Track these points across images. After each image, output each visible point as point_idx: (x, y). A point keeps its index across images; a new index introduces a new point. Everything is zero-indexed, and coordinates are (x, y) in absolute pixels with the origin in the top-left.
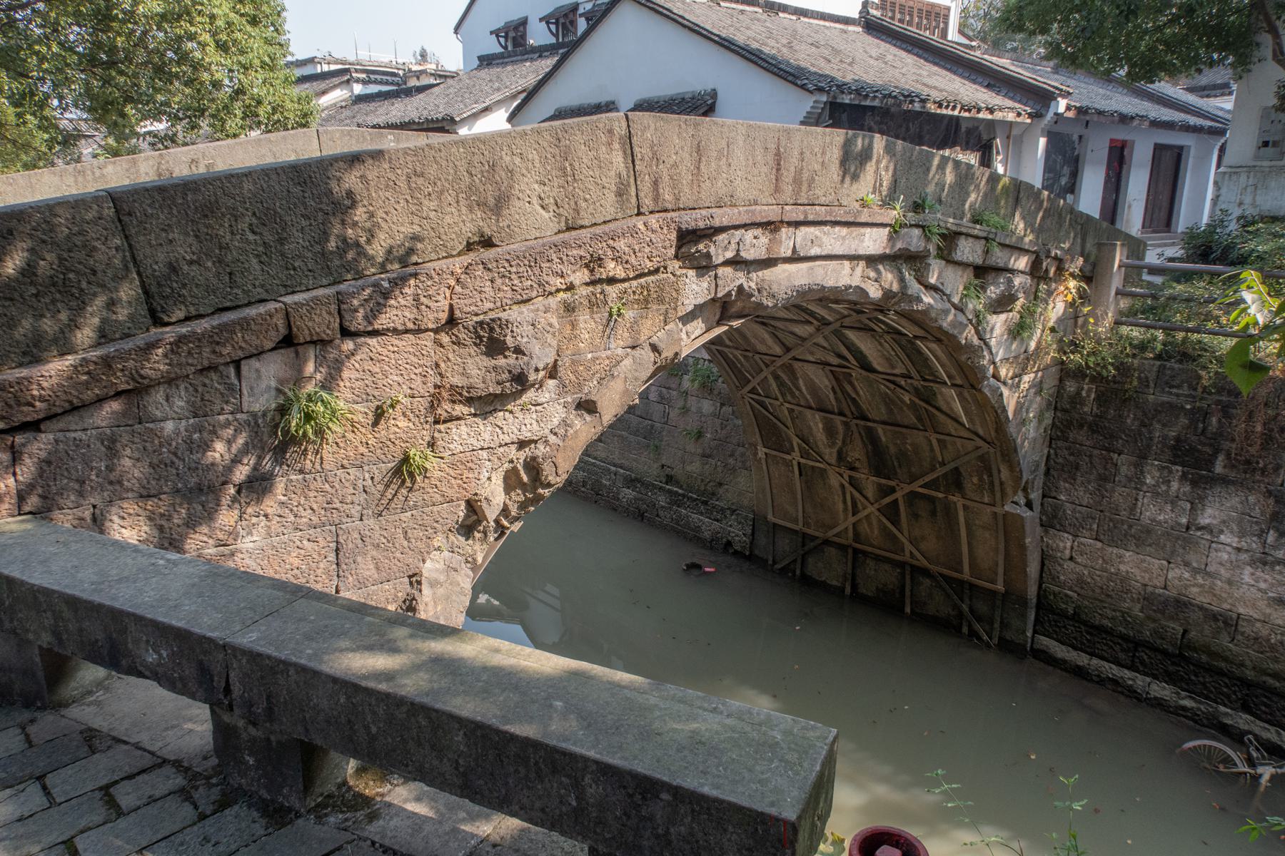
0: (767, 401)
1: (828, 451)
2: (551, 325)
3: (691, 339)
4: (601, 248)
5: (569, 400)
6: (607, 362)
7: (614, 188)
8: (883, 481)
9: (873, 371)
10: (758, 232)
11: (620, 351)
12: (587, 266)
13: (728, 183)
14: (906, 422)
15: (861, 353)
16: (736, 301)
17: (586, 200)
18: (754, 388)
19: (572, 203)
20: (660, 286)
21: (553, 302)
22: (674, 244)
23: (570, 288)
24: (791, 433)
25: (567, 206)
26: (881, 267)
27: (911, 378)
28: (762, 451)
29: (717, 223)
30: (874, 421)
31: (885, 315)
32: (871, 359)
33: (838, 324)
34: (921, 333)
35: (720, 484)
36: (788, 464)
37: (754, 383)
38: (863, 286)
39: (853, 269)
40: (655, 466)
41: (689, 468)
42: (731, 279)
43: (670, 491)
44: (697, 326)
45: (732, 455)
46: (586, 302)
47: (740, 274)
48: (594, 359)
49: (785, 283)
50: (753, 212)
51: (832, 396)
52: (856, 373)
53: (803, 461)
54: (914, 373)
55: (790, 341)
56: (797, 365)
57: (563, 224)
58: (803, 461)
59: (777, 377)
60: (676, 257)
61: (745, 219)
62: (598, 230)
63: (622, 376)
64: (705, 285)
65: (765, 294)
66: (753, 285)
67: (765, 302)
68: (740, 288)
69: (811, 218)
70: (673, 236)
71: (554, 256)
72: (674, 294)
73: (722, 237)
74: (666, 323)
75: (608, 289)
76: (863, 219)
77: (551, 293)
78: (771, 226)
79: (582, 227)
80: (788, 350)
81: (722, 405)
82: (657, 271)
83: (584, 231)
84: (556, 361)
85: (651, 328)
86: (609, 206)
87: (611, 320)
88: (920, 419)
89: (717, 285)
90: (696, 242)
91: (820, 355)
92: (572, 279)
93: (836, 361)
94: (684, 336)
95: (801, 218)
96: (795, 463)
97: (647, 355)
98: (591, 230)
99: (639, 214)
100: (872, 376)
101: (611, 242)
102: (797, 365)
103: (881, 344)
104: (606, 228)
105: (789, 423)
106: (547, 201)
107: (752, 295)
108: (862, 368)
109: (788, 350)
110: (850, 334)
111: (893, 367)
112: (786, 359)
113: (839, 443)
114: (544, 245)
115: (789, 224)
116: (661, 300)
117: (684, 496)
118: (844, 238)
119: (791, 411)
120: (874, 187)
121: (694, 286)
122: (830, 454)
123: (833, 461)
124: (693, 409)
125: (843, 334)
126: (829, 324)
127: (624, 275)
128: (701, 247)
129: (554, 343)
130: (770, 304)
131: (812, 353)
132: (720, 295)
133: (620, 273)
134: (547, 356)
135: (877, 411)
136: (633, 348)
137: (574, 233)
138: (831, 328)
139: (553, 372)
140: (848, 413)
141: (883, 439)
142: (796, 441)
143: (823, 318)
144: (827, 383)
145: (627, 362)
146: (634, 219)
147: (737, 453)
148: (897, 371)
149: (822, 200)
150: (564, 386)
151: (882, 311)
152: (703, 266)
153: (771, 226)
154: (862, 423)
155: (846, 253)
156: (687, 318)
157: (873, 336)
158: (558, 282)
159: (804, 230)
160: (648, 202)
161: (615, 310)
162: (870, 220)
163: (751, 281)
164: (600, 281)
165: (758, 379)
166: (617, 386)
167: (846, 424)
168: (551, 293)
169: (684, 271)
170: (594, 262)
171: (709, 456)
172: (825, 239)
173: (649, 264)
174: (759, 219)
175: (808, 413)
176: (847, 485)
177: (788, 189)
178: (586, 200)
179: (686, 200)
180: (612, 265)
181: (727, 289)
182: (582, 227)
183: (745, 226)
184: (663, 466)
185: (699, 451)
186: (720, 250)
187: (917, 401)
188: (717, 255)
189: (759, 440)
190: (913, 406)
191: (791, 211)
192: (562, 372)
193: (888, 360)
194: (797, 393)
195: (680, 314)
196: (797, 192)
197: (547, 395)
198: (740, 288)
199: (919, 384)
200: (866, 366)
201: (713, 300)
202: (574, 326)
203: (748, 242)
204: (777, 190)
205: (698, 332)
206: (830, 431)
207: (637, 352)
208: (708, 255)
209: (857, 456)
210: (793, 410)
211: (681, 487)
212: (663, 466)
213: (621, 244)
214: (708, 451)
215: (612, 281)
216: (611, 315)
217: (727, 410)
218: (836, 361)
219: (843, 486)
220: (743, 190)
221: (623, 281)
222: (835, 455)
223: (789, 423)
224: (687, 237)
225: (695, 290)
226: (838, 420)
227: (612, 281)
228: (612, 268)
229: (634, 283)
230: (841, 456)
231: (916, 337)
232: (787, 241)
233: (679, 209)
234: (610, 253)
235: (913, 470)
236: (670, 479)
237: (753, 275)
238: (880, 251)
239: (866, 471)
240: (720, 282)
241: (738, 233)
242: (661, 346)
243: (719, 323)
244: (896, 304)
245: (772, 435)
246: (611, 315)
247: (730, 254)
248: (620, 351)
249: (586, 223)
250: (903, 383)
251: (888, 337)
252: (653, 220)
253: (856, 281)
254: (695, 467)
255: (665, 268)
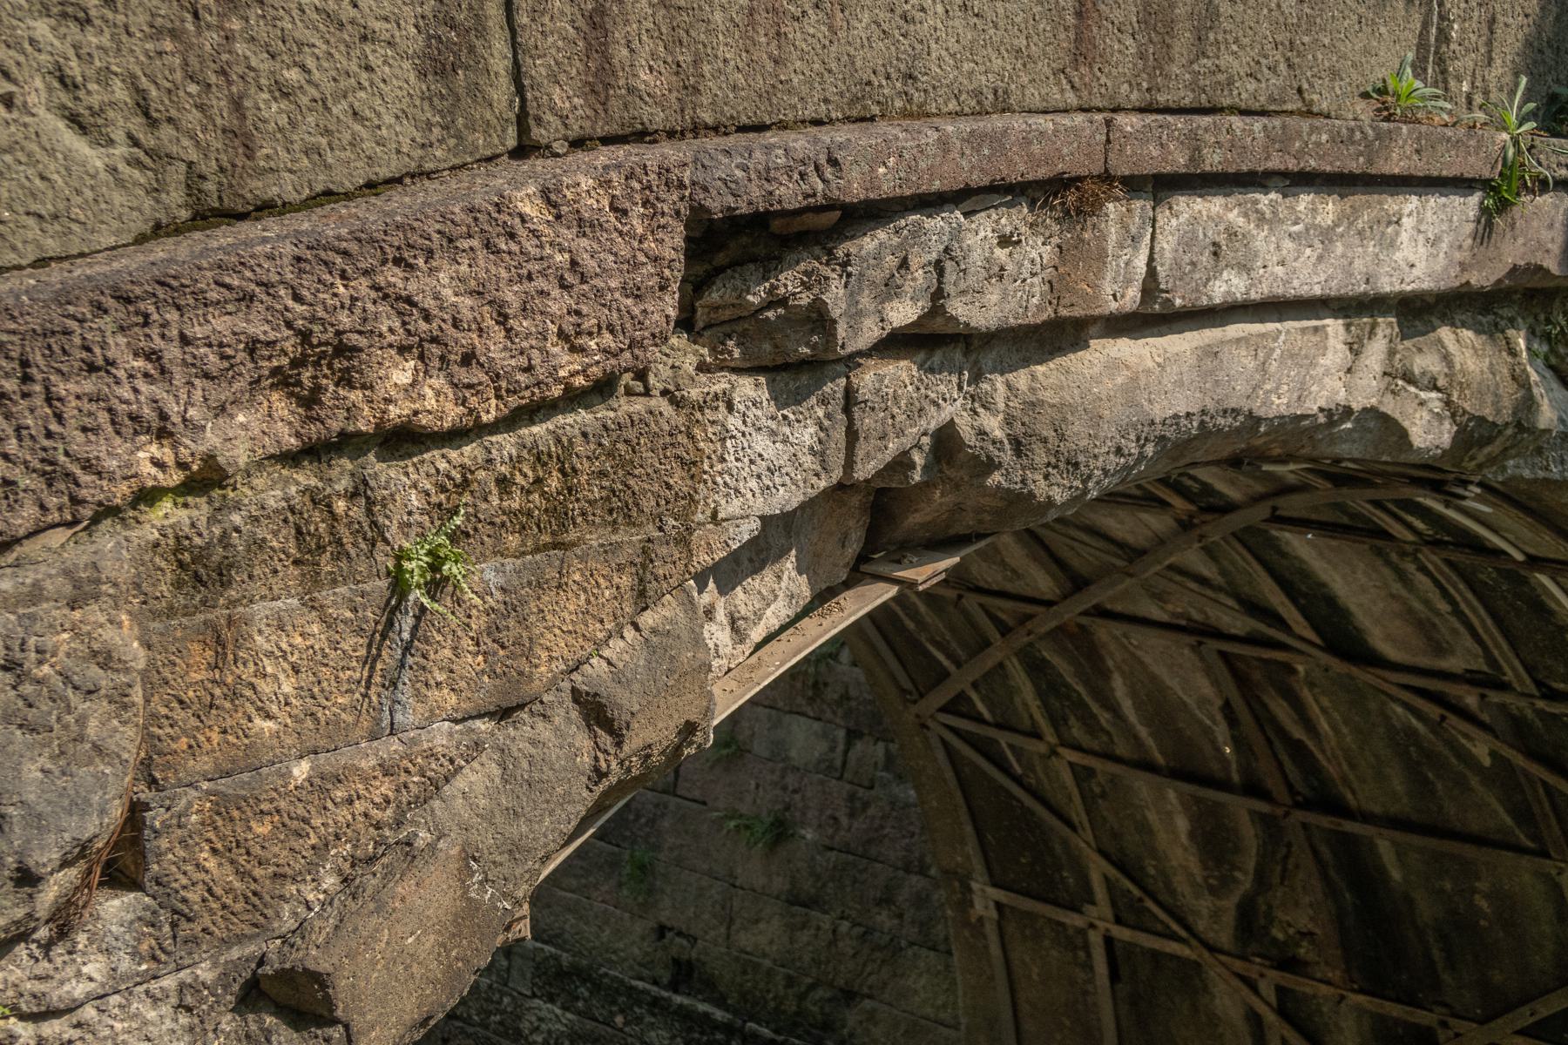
0: (1004, 739)
1: (1205, 904)
2: (106, 659)
3: (752, 638)
4: (343, 302)
5: (205, 972)
6: (385, 788)
7: (416, 43)
8: (1395, 1010)
9: (1373, 660)
10: (1014, 218)
11: (441, 736)
12: (283, 380)
13: (893, 24)
14: (1475, 825)
15: (1331, 601)
16: (926, 485)
17: (283, 91)
18: (961, 697)
19: (219, 103)
20: (619, 451)
21: (112, 548)
22: (676, 275)
23: (206, 479)
24: (1083, 844)
25: (192, 118)
26: (1445, 333)
27: (1503, 687)
28: (985, 898)
29: (854, 187)
30: (1366, 818)
31: (1451, 499)
32: (1363, 620)
33: (1263, 511)
34: (1548, 545)
35: (849, 996)
36: (1075, 942)
37: (961, 681)
38: (1389, 407)
39: (1355, 349)
40: (639, 927)
41: (745, 940)
42: (909, 405)
43: (685, 1015)
44: (781, 588)
45: (886, 900)
46: (281, 540)
47: (945, 385)
48: (321, 784)
49: (1115, 413)
50: (997, 140)
51: (1221, 731)
52: (1310, 663)
53: (1122, 934)
54: (1513, 670)
55: (1085, 556)
56: (1104, 632)
57: (175, 196)
58: (1122, 934)
59: (1037, 668)
60: (685, 323)
61: (967, 170)
62: (331, 224)
63: (450, 848)
64: (807, 435)
65: (1040, 457)
66: (993, 425)
67: (1040, 488)
68: (945, 441)
69: (1213, 160)
70: (672, 244)
71: (118, 347)
72: (678, 479)
73: (870, 242)
74: (643, 600)
75: (386, 473)
76: (1396, 163)
77: (107, 511)
78: (1061, 195)
79: (266, 208)
80: (1078, 583)
81: (853, 735)
82: (603, 388)
83: (272, 227)
84: (136, 810)
85: (583, 630)
86: (389, 112)
87: (395, 626)
88: (1524, 815)
89: (852, 435)
90: (770, 264)
91: (1186, 603)
92: (211, 439)
93: (1239, 624)
94: (718, 634)
95: (1179, 161)
96: (1095, 938)
97: (561, 741)
98: (304, 223)
99: (523, 150)
100: (1364, 676)
101: (392, 276)
102: (1104, 632)
103: (1402, 576)
104: (369, 213)
105: (1077, 812)
106: (95, 95)
107: (991, 465)
108: (1332, 648)
109: (1078, 583)
110: (1302, 546)
111: (1440, 650)
112: (1070, 612)
113: (1246, 882)
114: (64, 297)
115: (1134, 185)
116: (620, 509)
117: (729, 1029)
118: (1327, 235)
119: (1083, 775)
120: (1422, 46)
121: (761, 443)
122: (1215, 916)
123: (1225, 938)
124: (760, 748)
125: (1273, 544)
126: (1228, 508)
127: (453, 414)
128: (788, 281)
129: (127, 740)
130: (1059, 496)
131: (1160, 597)
132: (865, 470)
133: (436, 403)
134: (79, 806)
135: (1379, 787)
136: (503, 714)
137: (224, 237)
138: (1236, 520)
139: (122, 863)
140: (1273, 783)
141: (1396, 874)
142: (1098, 870)
143: (1207, 489)
144: (1207, 689)
145: (476, 778)
146: (500, 177)
147: (903, 896)
148: (1454, 664)
149: (1246, 92)
150: (180, 916)
151: (1437, 487)
152: (798, 361)
153: (1061, 195)
154: (1325, 821)
155: (1335, 288)
156: (732, 571)
157: (1379, 552)
158: (147, 459)
159: (1190, 208)
160: (562, 100)
161: (415, 567)
162: (1418, 167)
163: (981, 410)
164: (348, 443)
165: (975, 670)
166: (429, 895)
167: (1268, 824)
168: (107, 511)
169: (721, 383)
170: (318, 363)
171: (812, 903)
172: (1261, 240)
173: (567, 364)
174: (1019, 169)
175: (1142, 785)
176: (1270, 1017)
177: (1122, 51)
178: (283, 91)
179: (727, 86)
180: (402, 374)
181: (893, 446)
182: (266, 208)
183: (965, 198)
184: (662, 931)
185: (780, 884)
186: (869, 295)
187: (1519, 760)
188: (856, 315)
189: (978, 866)
190: (1502, 776)
191: (1142, 136)
192: (166, 855)
193: (1425, 627)
194: (1104, 717)
195: (703, 559)
196: (1155, 63)
197: (95, 967)
198: (945, 441)
199: (1529, 707)
200: (1343, 640)
201: (840, 486)
202: (223, 644)
203: (976, 257)
204: (1082, 52)
205: (776, 614)
206: (1214, 841)
207: (523, 733)
208: (819, 319)
209: (1303, 921)
210: (1091, 772)
211: (720, 1002)
212: (662, 931)
213: (442, 285)
214: (807, 886)
215: (402, 440)
216: (399, 585)
217: (871, 751)
218: (1239, 624)
219: (1254, 1019)
220: (950, 52)
221: (455, 436)
222: (1229, 918)
223: (1077, 812)
224: (727, 243)
225: (766, 454)
226: (1241, 809)
227: (402, 440)
228: (402, 387)
229: (506, 444)
230: (1249, 922)
231: (1534, 561)
232: (1132, 248)
233: (697, 129)
234: (387, 322)
235: (1497, 977)
236: (684, 974)
237: (996, 386)
238: (1451, 282)
239: (1335, 975)
240: (866, 422)
241: (936, 224)
242: (625, 701)
243: (858, 574)
244: (1492, 460)
245: (1022, 849)
246: (399, 585)
247: (903, 313)
248: (441, 736)
249: (286, 188)
250: (1471, 700)
251: (1432, 559)
252: (583, 178)
253: (1366, 391)
254: (765, 936)
255: (641, 375)
